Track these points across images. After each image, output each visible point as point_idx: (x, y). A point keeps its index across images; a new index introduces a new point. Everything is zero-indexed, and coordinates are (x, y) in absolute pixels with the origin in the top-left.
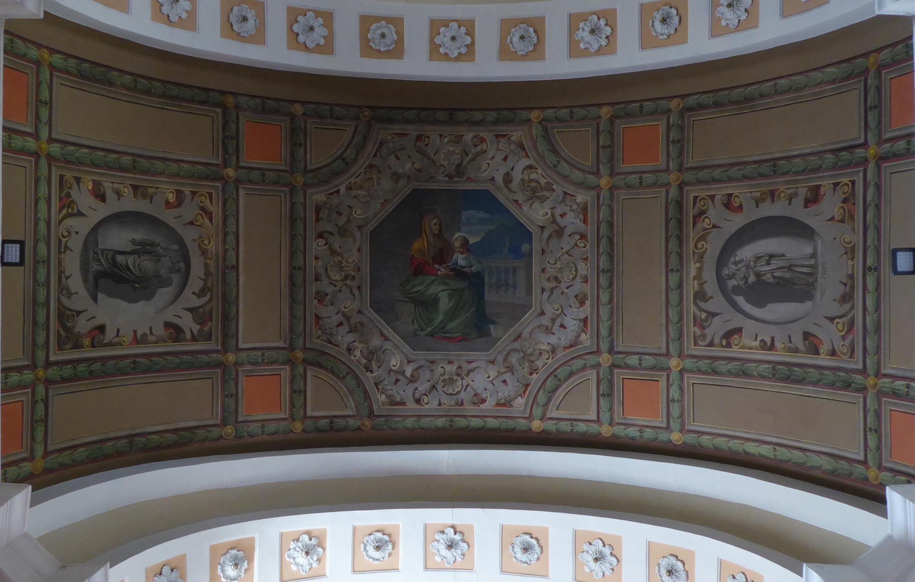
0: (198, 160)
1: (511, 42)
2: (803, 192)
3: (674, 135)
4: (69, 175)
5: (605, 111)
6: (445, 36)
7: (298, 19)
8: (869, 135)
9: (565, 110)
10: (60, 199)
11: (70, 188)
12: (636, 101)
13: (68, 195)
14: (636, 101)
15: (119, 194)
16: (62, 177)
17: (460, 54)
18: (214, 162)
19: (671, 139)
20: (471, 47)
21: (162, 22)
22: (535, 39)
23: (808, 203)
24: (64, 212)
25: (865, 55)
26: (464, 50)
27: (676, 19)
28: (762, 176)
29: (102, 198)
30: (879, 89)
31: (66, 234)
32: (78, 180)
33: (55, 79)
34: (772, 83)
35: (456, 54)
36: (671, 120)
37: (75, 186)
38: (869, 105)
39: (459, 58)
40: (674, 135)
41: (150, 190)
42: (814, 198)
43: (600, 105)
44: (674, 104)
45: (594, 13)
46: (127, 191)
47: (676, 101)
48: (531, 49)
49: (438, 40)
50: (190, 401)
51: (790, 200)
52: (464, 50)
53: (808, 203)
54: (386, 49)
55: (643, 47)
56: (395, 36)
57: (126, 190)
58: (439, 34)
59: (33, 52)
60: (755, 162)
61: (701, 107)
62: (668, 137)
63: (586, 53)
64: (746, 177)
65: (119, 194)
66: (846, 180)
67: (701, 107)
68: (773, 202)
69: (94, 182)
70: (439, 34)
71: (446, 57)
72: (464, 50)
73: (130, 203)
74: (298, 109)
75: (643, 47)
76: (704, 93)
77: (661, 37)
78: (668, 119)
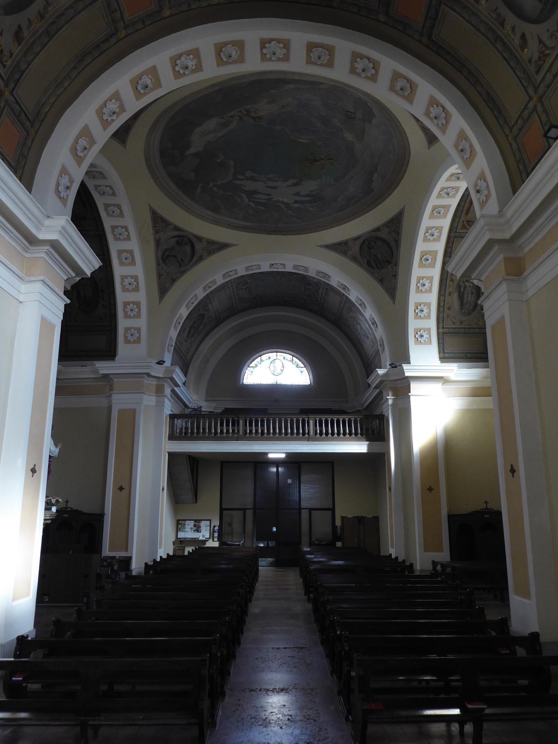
0: (456, 15)
1: (237, 52)
2: (26, 33)
3: (118, 15)
4: (532, 69)
5: (167, 13)
6: (280, 53)
7: (371, 76)
8: (13, 99)
9: (194, 7)
10: (544, 61)
11: (536, 62)
12: (149, 25)
13: (540, 58)
14: (149, 25)
15: (513, 29)
16: (537, 72)
17: (270, 43)
18: (448, 8)
19: (118, 11)
20: (263, 47)
21: (447, 110)
22: (222, 54)
23: (20, 28)
24: (547, 52)
25: (37, 132)
26: (267, 45)
27: (139, 88)
28: (53, 23)
29: (523, 36)
30: (23, 125)
31: (554, 37)
32: (530, 61)
33: (513, 123)
34: (72, 79)
35: (272, 43)
36: (122, 23)
37: (533, 60)
38: (22, 113)
39: (270, 41)
40: (118, 15)
41: (494, 16)
42: (18, 36)
43: (171, 16)
44: (123, 33)
45: (187, 75)
46: (508, 27)
47: (123, 35)
48: (223, 49)
49: (285, 51)
50: (441, 326)
51: (30, 22)
52: (267, 45)
53: (20, 28)
54: (318, 49)
55: (154, 67)
56: (312, 55)
57: (508, 28)
58: (283, 54)
59: (514, 145)
60: (60, 29)
61: (107, 40)
62: (121, 12)
63: (188, 53)
64: (63, 14)
65: (513, 29)
66: (8, 63)
67: (107, 40)
68: (39, 12)
69: (523, 51)
70: (283, 54)
71: (279, 41)
72: (267, 45)
73: (511, 19)
74: (382, 18)
75: (154, 67)
76: (108, 49)
77: (145, 76)
78: (124, 23)
